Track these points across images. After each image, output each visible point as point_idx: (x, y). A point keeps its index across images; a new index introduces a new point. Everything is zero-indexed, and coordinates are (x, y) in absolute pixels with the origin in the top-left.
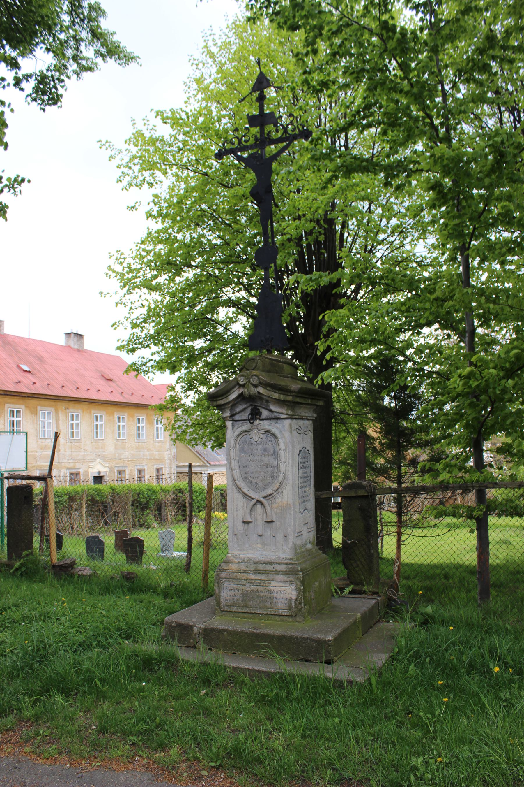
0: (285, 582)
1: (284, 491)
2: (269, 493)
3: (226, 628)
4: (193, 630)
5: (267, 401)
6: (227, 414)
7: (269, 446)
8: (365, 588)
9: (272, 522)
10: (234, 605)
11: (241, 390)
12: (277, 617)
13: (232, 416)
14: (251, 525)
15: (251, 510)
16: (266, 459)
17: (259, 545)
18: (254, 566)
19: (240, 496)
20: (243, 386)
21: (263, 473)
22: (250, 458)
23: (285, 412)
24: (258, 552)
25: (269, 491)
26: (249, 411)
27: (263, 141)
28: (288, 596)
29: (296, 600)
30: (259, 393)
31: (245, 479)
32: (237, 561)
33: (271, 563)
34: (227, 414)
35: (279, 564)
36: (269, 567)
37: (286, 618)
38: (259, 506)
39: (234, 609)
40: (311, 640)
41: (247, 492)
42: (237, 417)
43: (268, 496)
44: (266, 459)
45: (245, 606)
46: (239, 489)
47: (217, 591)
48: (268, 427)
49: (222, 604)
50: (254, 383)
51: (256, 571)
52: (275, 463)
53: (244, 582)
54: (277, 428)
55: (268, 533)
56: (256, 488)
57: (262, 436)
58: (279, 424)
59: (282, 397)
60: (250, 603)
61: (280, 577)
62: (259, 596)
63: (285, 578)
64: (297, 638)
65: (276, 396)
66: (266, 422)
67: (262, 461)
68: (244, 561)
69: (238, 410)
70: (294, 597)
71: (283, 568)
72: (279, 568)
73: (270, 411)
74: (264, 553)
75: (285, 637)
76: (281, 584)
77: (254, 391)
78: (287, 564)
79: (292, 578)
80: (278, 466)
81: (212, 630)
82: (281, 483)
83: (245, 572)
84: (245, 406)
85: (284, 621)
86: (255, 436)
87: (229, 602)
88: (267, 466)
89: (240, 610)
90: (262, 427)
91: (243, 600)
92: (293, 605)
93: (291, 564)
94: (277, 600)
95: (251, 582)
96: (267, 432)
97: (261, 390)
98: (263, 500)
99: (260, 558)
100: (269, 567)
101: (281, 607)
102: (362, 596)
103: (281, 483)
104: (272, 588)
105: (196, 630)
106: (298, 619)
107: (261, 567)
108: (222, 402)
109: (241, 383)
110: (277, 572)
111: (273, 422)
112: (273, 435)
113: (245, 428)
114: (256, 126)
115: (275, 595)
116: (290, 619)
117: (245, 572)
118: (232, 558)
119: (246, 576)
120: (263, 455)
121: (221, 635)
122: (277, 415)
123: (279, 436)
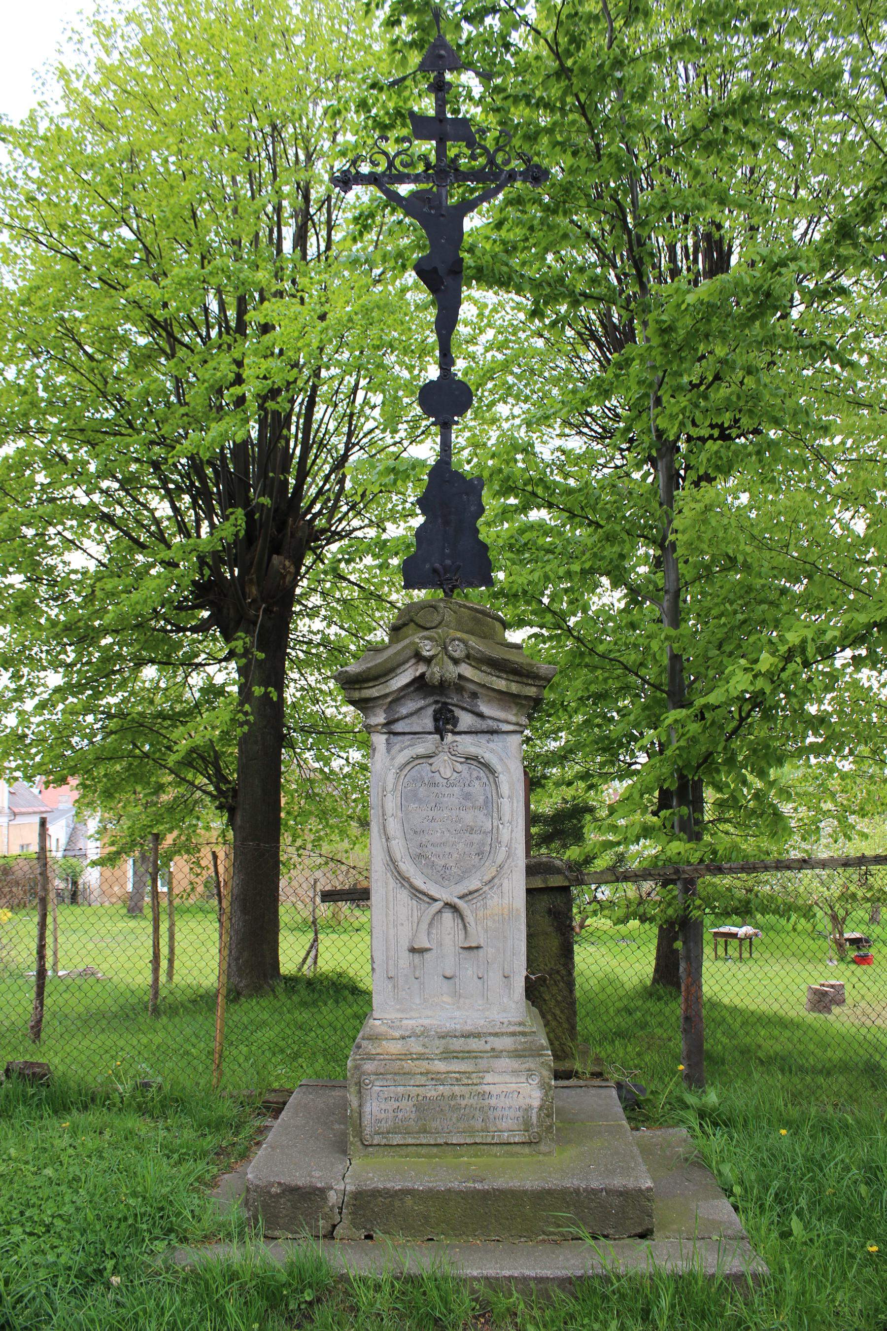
0: (515, 1072)
1: (506, 883)
2: (472, 887)
3: (409, 1185)
4: (325, 1199)
5: (474, 695)
6: (380, 718)
7: (476, 788)
8: (578, 1066)
9: (478, 948)
10: (394, 1131)
11: (422, 669)
12: (495, 1149)
13: (388, 723)
14: (427, 955)
15: (431, 924)
16: (468, 817)
17: (446, 998)
18: (438, 1046)
19: (404, 895)
20: (428, 661)
21: (460, 846)
22: (431, 814)
23: (513, 719)
24: (444, 1013)
25: (475, 884)
26: (430, 711)
27: (444, 171)
28: (522, 1102)
29: (541, 1108)
30: (460, 677)
31: (418, 858)
32: (397, 1034)
33: (477, 1035)
34: (380, 718)
35: (496, 1035)
36: (475, 1044)
37: (517, 1148)
38: (448, 916)
39: (397, 1140)
40: (608, 1192)
41: (423, 887)
42: (399, 727)
43: (471, 893)
44: (468, 817)
45: (423, 1134)
46: (403, 879)
47: (355, 1103)
48: (473, 750)
49: (368, 1131)
50: (456, 655)
51: (448, 1055)
52: (488, 826)
53: (422, 1080)
54: (492, 751)
55: (469, 971)
56: (443, 876)
57: (459, 767)
58: (497, 743)
59: (514, 688)
60: (436, 1124)
61: (505, 1063)
62: (458, 1108)
63: (515, 1064)
64: (577, 1191)
65: (501, 684)
66: (467, 739)
67: (460, 820)
68: (414, 1034)
69: (404, 711)
70: (536, 1103)
71: (506, 1043)
72: (500, 1043)
73: (480, 715)
74: (457, 1014)
75: (549, 1192)
76: (508, 1078)
77: (453, 671)
78: (513, 1034)
79: (531, 1063)
80: (494, 833)
81: (376, 1193)
82: (501, 867)
83: (421, 1057)
84: (422, 703)
85: (512, 1155)
86: (444, 765)
87: (384, 1126)
88: (471, 830)
89: (410, 1141)
90: (460, 749)
91: (419, 1119)
92: (534, 1120)
93: (523, 1034)
94: (499, 1113)
95: (437, 1079)
96: (470, 759)
97: (466, 670)
98: (460, 903)
99: (449, 1026)
100: (475, 1044)
101: (507, 1126)
102: (572, 1082)
103: (501, 867)
104: (487, 1088)
105: (333, 1198)
106: (543, 1148)
107: (457, 1044)
108: (374, 692)
109: (426, 654)
110: (496, 1054)
111: (483, 739)
112: (487, 766)
113: (420, 749)
114: (430, 138)
115: (493, 1102)
116: (526, 1150)
117: (421, 1057)
118: (383, 1029)
119: (424, 1065)
120: (464, 808)
121: (397, 1203)
122: (493, 725)
123: (498, 767)
